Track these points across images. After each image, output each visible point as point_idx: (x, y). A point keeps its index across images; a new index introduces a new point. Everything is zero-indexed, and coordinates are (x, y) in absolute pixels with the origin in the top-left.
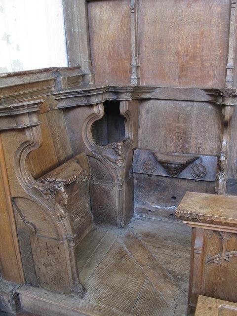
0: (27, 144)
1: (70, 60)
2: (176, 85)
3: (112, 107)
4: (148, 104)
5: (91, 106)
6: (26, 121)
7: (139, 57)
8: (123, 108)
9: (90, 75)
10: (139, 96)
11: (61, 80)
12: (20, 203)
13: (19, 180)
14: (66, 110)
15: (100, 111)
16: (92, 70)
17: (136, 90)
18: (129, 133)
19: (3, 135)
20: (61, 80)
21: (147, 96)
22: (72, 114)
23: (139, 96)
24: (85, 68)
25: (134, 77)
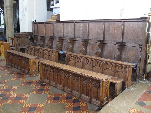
1: (32, 31)
3: (32, 37)
6: (17, 37)
8: (33, 38)
14: (27, 37)
15: (30, 38)
17: (35, 36)
18: (35, 41)
24: (33, 33)
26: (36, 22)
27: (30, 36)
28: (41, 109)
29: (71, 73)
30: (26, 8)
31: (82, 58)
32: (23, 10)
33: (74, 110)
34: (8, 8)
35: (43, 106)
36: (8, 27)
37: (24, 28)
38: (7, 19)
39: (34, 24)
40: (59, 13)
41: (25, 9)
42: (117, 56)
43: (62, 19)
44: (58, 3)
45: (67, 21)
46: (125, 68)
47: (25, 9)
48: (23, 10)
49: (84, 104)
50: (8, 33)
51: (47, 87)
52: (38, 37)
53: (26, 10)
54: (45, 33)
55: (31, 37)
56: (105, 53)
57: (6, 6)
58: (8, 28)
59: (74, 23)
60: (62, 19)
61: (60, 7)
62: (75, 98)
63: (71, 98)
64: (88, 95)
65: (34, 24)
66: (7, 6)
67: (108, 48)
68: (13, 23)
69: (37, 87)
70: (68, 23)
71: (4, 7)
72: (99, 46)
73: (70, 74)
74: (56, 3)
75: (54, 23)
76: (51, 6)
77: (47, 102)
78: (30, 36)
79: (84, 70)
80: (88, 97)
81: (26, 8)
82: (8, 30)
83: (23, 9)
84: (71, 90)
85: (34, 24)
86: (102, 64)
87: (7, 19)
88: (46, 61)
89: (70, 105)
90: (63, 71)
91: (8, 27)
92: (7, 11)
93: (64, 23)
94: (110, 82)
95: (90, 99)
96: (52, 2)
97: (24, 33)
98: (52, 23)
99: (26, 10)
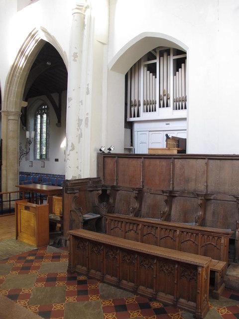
0: (75, 197)
1: (98, 175)
2: (128, 186)
3: (104, 191)
4: (119, 192)
5: (98, 190)
6: (76, 191)
7: (117, 174)
8: (108, 192)
9: (103, 181)
10: (115, 189)
11: (90, 182)
12: (72, 212)
13: (72, 258)
14: (92, 191)
15: (100, 192)
16: (104, 179)
17: (113, 187)
18: (111, 201)
19: (106, 3)
20: (90, 182)
21: (119, 189)
22: (92, 193)
23: (115, 189)
24: (102, 178)
25: (115, 182)
26: (111, 152)
27: (101, 188)
28: (60, 313)
29: (104, 244)
30: (87, 119)
31: (178, 230)
32: (79, 125)
33: (117, 311)
34: (11, 117)
35: (62, 308)
36: (7, 159)
37: (78, 167)
38: (7, 140)
39: (104, 158)
40: (181, 135)
41: (83, 122)
42: (164, 213)
43: (190, 150)
44: (151, 112)
45: (223, 156)
46: (219, 238)
47: (83, 122)
48: (79, 125)
49: (130, 300)
50: (7, 174)
51: (37, 264)
52: (175, 196)
53: (87, 124)
54: (143, 182)
55: (103, 190)
56: (144, 210)
57: (8, 112)
58: (7, 163)
59: (206, 160)
60: (190, 150)
61: (185, 119)
62: (82, 278)
63: (74, 278)
64: (152, 287)
65: (104, 158)
66: (8, 113)
67: (148, 200)
68: (19, 151)
69: (19, 265)
70: (223, 161)
71: (2, 113)
72: (136, 198)
73: (101, 246)
74: (176, 109)
75: (175, 158)
76: (131, 117)
77: (36, 285)
78: (101, 188)
79: (106, 236)
80: (84, 268)
81: (87, 119)
82: (6, 166)
83: (80, 121)
84: (177, 298)
85: (104, 157)
86: (140, 226)
87: (7, 140)
88: (161, 249)
89: (71, 288)
90: (157, 260)
91: (7, 159)
92: (7, 125)
93: (209, 159)
94: (211, 271)
95: (175, 300)
96: (133, 109)
97: (77, 182)
98: (171, 158)
99: (87, 124)
